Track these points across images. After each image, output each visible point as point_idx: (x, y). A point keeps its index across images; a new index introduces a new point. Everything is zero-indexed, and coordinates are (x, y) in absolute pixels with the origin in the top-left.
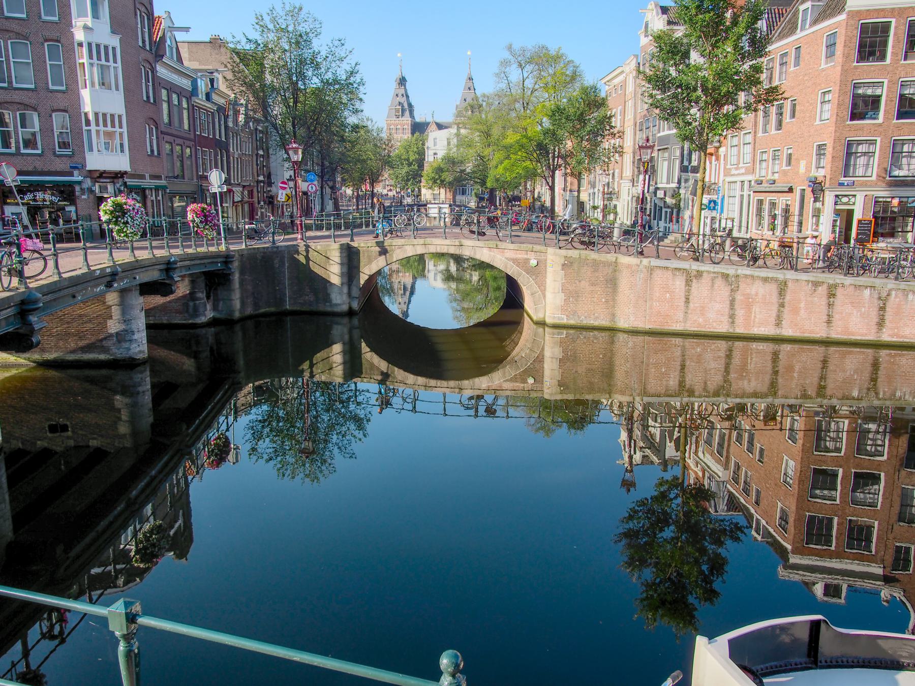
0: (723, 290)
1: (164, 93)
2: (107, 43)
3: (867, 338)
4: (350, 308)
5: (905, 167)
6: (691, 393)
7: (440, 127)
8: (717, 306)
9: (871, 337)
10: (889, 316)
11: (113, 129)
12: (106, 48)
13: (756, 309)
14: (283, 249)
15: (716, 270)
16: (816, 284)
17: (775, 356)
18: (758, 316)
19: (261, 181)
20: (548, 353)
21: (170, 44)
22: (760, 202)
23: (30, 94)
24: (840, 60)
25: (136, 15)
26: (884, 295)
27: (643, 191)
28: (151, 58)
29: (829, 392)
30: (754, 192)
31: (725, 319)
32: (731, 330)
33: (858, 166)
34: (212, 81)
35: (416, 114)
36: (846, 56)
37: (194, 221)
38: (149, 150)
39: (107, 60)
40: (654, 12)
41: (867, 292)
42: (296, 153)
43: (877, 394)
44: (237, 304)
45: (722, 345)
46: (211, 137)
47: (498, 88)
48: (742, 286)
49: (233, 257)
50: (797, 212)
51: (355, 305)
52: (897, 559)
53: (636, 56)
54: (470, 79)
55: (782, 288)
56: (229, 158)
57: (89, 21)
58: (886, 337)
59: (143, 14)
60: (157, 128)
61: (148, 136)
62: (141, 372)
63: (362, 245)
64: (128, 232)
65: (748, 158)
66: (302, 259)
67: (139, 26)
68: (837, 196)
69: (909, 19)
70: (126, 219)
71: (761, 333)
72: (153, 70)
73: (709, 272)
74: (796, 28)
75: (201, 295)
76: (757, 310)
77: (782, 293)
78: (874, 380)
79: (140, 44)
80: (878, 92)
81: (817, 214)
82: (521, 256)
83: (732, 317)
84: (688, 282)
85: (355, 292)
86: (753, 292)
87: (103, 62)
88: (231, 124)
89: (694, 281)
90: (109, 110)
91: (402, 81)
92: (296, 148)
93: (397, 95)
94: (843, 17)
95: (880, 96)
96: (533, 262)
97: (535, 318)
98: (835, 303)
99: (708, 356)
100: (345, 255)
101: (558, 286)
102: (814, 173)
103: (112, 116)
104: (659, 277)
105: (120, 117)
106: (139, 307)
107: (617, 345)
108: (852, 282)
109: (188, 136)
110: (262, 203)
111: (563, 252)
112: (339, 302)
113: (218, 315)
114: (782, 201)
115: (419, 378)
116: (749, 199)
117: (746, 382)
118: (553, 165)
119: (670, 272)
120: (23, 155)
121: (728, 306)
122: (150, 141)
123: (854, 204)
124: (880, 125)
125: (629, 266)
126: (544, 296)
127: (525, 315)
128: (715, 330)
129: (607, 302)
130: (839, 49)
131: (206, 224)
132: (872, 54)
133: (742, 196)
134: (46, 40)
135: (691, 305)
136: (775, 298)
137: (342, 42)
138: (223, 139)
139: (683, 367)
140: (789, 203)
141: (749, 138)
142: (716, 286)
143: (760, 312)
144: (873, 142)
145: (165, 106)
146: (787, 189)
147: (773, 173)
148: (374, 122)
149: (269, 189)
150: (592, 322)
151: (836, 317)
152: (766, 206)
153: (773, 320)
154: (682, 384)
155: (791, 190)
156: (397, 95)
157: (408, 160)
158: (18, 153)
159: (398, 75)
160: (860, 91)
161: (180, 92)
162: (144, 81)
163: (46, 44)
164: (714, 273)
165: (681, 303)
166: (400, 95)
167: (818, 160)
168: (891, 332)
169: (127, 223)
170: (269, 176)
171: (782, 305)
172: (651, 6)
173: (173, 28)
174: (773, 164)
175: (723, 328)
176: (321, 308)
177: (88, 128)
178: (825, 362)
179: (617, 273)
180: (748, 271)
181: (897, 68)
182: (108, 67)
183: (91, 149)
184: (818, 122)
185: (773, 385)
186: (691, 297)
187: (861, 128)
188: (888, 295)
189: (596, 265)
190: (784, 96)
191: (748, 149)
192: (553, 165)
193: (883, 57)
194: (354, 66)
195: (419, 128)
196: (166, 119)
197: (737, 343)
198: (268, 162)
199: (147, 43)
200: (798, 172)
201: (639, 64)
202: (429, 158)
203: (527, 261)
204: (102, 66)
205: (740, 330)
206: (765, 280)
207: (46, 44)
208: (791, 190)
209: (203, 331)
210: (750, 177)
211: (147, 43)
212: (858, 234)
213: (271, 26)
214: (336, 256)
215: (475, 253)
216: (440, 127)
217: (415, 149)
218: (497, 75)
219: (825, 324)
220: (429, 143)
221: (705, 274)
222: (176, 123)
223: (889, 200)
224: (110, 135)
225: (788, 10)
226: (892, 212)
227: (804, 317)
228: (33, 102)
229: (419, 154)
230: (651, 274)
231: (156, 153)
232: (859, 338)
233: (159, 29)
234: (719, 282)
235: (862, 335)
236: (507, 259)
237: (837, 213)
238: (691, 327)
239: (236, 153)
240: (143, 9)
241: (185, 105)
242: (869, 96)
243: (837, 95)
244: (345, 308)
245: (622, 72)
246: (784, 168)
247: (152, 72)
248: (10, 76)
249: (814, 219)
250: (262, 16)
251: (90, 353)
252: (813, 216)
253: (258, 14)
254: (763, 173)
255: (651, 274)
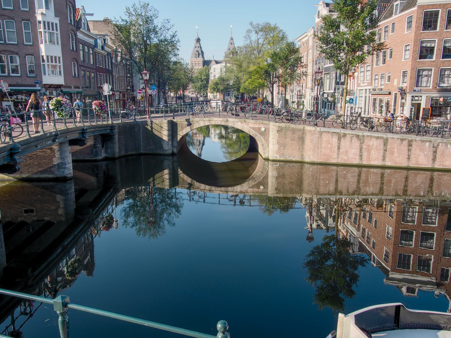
0: (356, 143)
1: (81, 46)
2: (53, 21)
3: (427, 166)
4: (173, 152)
5: (446, 82)
6: (341, 193)
7: (217, 62)
8: (354, 151)
9: (429, 166)
10: (438, 156)
11: (56, 64)
12: (52, 24)
13: (373, 152)
14: (140, 123)
15: (353, 133)
16: (402, 140)
17: (382, 175)
18: (373, 156)
19: (129, 89)
20: (270, 174)
21: (84, 22)
22: (375, 100)
23: (15, 47)
24: (414, 30)
25: (67, 7)
26: (436, 145)
27: (317, 94)
28: (74, 29)
29: (409, 193)
30: (372, 94)
31: (357, 157)
32: (360, 163)
33: (423, 82)
34: (105, 40)
35: (205, 56)
36: (417, 27)
37: (95, 109)
38: (73, 74)
39: (53, 30)
40: (323, 6)
41: (427, 144)
42: (146, 75)
43: (432, 194)
44: (117, 150)
45: (356, 170)
46: (104, 67)
47: (245, 44)
48: (366, 141)
49: (115, 127)
50: (393, 104)
51: (175, 151)
52: (442, 275)
53: (314, 28)
54: (232, 39)
55: (386, 142)
56: (113, 78)
57: (44, 10)
58: (437, 166)
59: (71, 7)
60: (77, 63)
61: (73, 67)
62: (70, 184)
63: (179, 121)
64: (63, 114)
65: (369, 78)
66: (149, 128)
67: (69, 13)
68: (412, 96)
69: (448, 9)
70: (62, 108)
71: (375, 164)
72: (76, 35)
73: (349, 134)
74: (392, 14)
75: (99, 145)
76: (373, 153)
77: (385, 144)
78: (431, 187)
79: (69, 22)
80: (433, 45)
81: (403, 105)
82: (257, 126)
83: (361, 156)
84: (339, 139)
85: (175, 144)
86: (371, 144)
87: (51, 31)
88: (114, 61)
89: (342, 138)
90: (54, 55)
91: (198, 40)
92: (146, 73)
93: (196, 47)
94: (415, 8)
95: (434, 47)
96: (263, 129)
97: (264, 157)
98: (412, 149)
99: (349, 175)
100: (170, 126)
101: (275, 141)
102: (401, 85)
103: (55, 57)
104: (325, 137)
105: (59, 58)
106: (69, 152)
107: (304, 170)
108: (420, 139)
109: (93, 67)
110: (129, 100)
111: (278, 124)
112: (167, 149)
113: (107, 156)
114: (385, 99)
115: (207, 186)
116: (369, 98)
117: (368, 188)
118: (273, 81)
119: (330, 134)
120: (11, 76)
121: (359, 151)
122: (74, 70)
123: (421, 100)
124: (434, 61)
125: (310, 131)
126: (268, 146)
127: (259, 155)
128: (353, 163)
129: (299, 149)
130: (414, 24)
131: (102, 111)
132: (430, 26)
133: (366, 96)
134: (23, 20)
135: (341, 150)
136: (382, 147)
137: (169, 21)
138: (110, 69)
139: (337, 181)
140: (389, 100)
141: (369, 68)
142: (353, 141)
143: (375, 154)
144: (431, 70)
145: (81, 52)
146: (388, 93)
147: (381, 85)
148: (184, 60)
149: (132, 93)
150: (292, 159)
151: (412, 156)
152: (378, 102)
153: (381, 157)
154: (336, 189)
155: (390, 93)
156: (196, 47)
157: (201, 79)
158: (9, 76)
159: (196, 37)
160: (424, 45)
161: (89, 46)
162: (71, 40)
163: (23, 22)
164: (352, 134)
165: (336, 149)
166: (197, 47)
167: (404, 79)
168: (439, 164)
169: (63, 110)
170: (133, 87)
171: (386, 150)
172: (321, 3)
173: (85, 14)
174: (381, 81)
175: (356, 161)
176: (159, 152)
177: (43, 63)
178: (407, 178)
179: (304, 134)
180: (369, 134)
181: (442, 33)
182: (53, 33)
183: (45, 74)
184: (403, 60)
185: (381, 189)
186: (341, 146)
187: (424, 63)
188: (438, 145)
189: (294, 131)
190: (386, 47)
191: (369, 73)
192: (273, 81)
193: (435, 28)
194: (174, 32)
195: (206, 63)
196: (82, 59)
197: (364, 169)
198: (132, 80)
199: (73, 21)
200: (393, 85)
201: (315, 31)
202: (212, 78)
203: (260, 128)
204: (50, 33)
205: (365, 163)
206: (377, 138)
207: (23, 22)
208: (390, 93)
209: (100, 163)
210: (368, 88)
211: (73, 21)
212: (423, 115)
213: (133, 13)
214: (165, 126)
215: (234, 125)
216: (217, 62)
217: (205, 74)
218: (245, 37)
219: (407, 160)
220: (212, 71)
221: (347, 135)
222: (87, 61)
223: (438, 98)
224: (54, 67)
225: (388, 5)
226: (440, 104)
227: (396, 156)
228: (16, 50)
229: (206, 76)
230: (321, 135)
231: (77, 76)
232: (424, 166)
233: (79, 14)
234: (355, 139)
235: (425, 165)
236: (250, 128)
237: (413, 105)
238: (341, 161)
239: (117, 76)
240: (71, 5)
241: (91, 52)
242: (429, 47)
243: (412, 47)
244: (170, 152)
245: (307, 35)
246: (386, 82)
247: (75, 36)
248: (5, 38)
249: (401, 108)
250: (129, 8)
251: (44, 174)
252: (401, 106)
253: (127, 7)
254: (376, 85)
255: (321, 135)
